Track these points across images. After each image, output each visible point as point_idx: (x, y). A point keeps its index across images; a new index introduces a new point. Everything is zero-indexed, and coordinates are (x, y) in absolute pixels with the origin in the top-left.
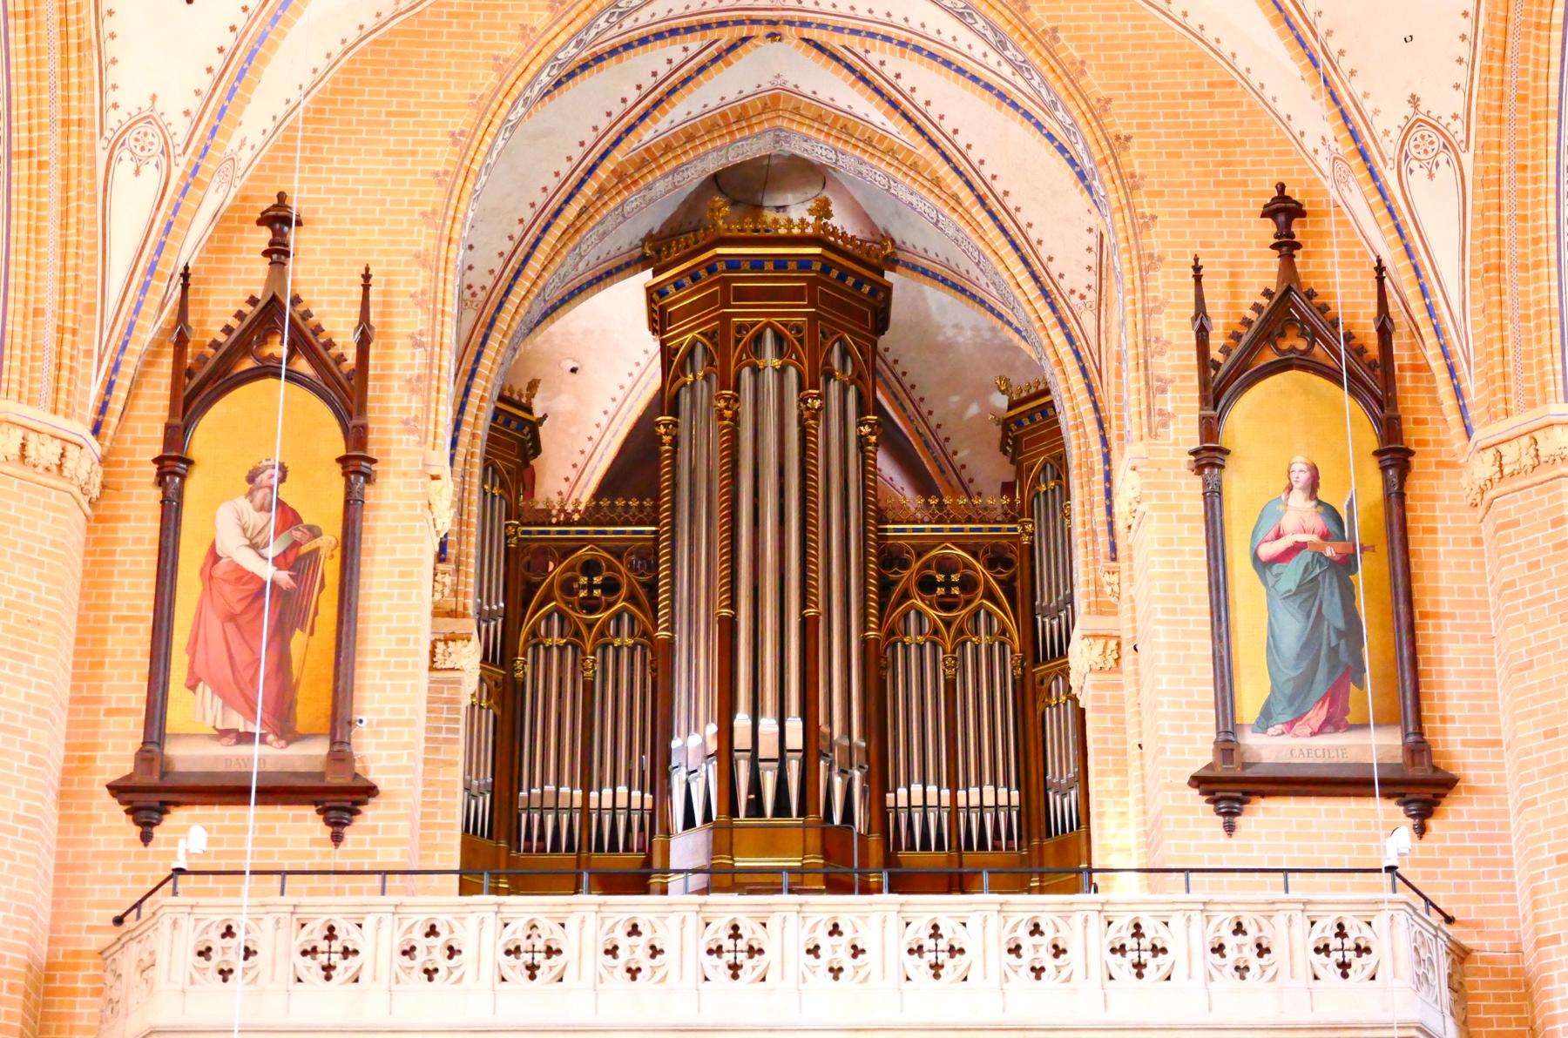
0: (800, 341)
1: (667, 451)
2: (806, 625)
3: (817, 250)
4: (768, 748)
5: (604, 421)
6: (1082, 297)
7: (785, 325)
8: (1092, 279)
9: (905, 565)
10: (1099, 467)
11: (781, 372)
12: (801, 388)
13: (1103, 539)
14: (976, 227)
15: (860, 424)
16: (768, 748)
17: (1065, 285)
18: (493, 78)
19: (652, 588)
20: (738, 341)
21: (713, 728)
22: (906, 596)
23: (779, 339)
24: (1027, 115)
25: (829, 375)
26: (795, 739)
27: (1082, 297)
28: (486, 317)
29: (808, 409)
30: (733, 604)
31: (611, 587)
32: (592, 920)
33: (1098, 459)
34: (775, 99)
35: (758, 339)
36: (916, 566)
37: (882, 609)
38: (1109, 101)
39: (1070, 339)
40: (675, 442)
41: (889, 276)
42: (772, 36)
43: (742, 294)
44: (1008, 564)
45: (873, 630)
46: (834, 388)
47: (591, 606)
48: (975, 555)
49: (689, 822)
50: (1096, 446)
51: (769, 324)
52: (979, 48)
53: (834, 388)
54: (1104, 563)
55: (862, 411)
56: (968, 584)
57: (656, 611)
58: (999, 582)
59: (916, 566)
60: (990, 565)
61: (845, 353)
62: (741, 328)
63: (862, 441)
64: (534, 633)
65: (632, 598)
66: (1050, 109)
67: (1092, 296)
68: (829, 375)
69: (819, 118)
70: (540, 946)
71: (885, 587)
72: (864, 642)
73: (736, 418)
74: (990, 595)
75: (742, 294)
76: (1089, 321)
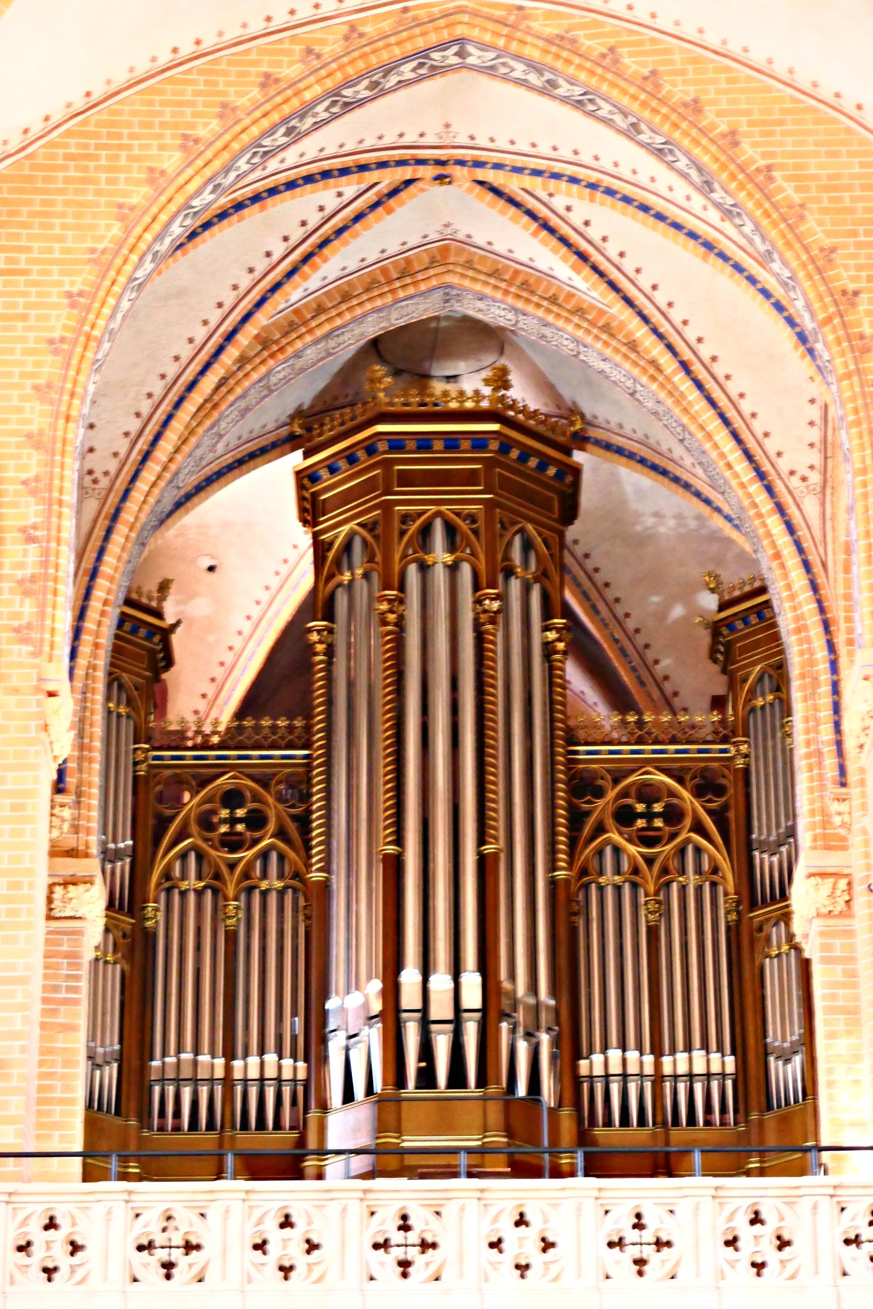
0: (475, 532)
1: (321, 662)
2: (484, 864)
3: (495, 427)
4: (441, 1009)
5: (247, 627)
6: (804, 479)
7: (458, 514)
8: (815, 458)
9: (599, 793)
10: (825, 677)
11: (453, 569)
12: (477, 587)
13: (830, 762)
14: (679, 398)
15: (546, 629)
16: (441, 1009)
17: (783, 465)
18: (116, 229)
19: (304, 822)
20: (403, 533)
21: (376, 985)
22: (600, 829)
23: (451, 530)
24: (738, 268)
25: (509, 572)
26: (472, 997)
27: (804, 479)
28: (109, 508)
29: (485, 611)
30: (399, 841)
31: (256, 821)
32: (237, 1208)
33: (823, 667)
34: (445, 251)
35: (426, 531)
36: (611, 794)
37: (573, 844)
38: (833, 250)
39: (791, 528)
40: (330, 652)
41: (579, 457)
42: (440, 178)
43: (406, 479)
44: (720, 791)
45: (563, 869)
46: (515, 586)
47: (233, 843)
48: (680, 781)
49: (348, 1096)
50: (821, 654)
51: (438, 514)
52: (682, 190)
53: (515, 586)
54: (832, 789)
55: (547, 613)
56: (673, 815)
57: (309, 848)
58: (710, 812)
59: (611, 794)
60: (698, 792)
61: (528, 546)
62: (406, 518)
63: (548, 649)
64: (167, 875)
65: (281, 834)
66: (765, 260)
67: (815, 478)
68: (509, 572)
69: (495, 273)
70: (178, 1240)
71: (576, 819)
72: (553, 884)
73: (400, 624)
74: (699, 828)
75: (406, 479)
76: (811, 506)
